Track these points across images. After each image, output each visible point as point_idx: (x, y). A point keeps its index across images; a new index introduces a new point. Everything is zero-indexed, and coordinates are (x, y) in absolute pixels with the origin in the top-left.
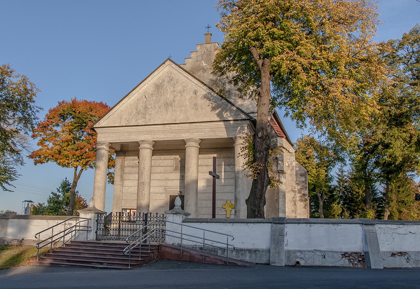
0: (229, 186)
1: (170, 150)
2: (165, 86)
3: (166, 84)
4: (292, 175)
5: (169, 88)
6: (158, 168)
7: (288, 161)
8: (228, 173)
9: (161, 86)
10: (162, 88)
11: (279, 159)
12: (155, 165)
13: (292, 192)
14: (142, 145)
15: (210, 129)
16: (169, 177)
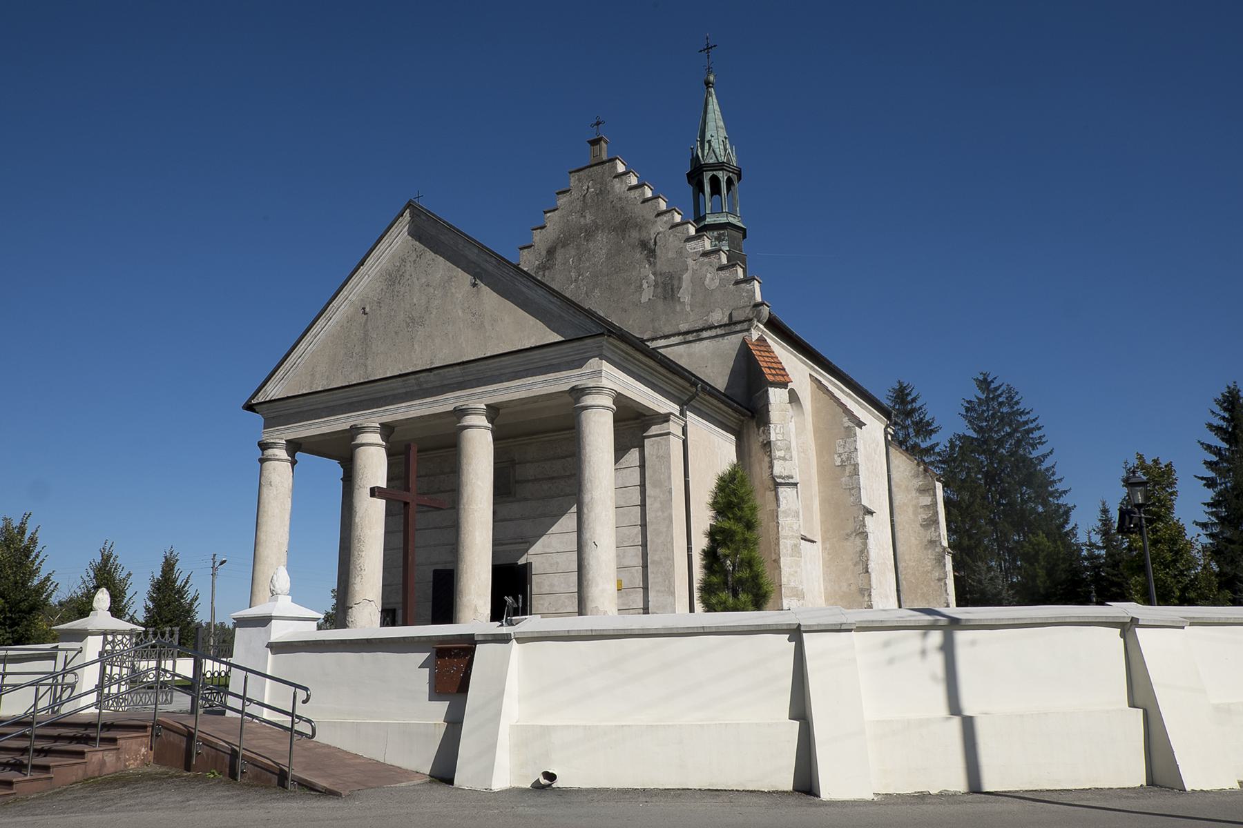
2: (407, 276)
3: (409, 269)
4: (853, 489)
5: (416, 279)
7: (841, 451)
9: (398, 276)
10: (402, 282)
11: (775, 445)
13: (858, 537)
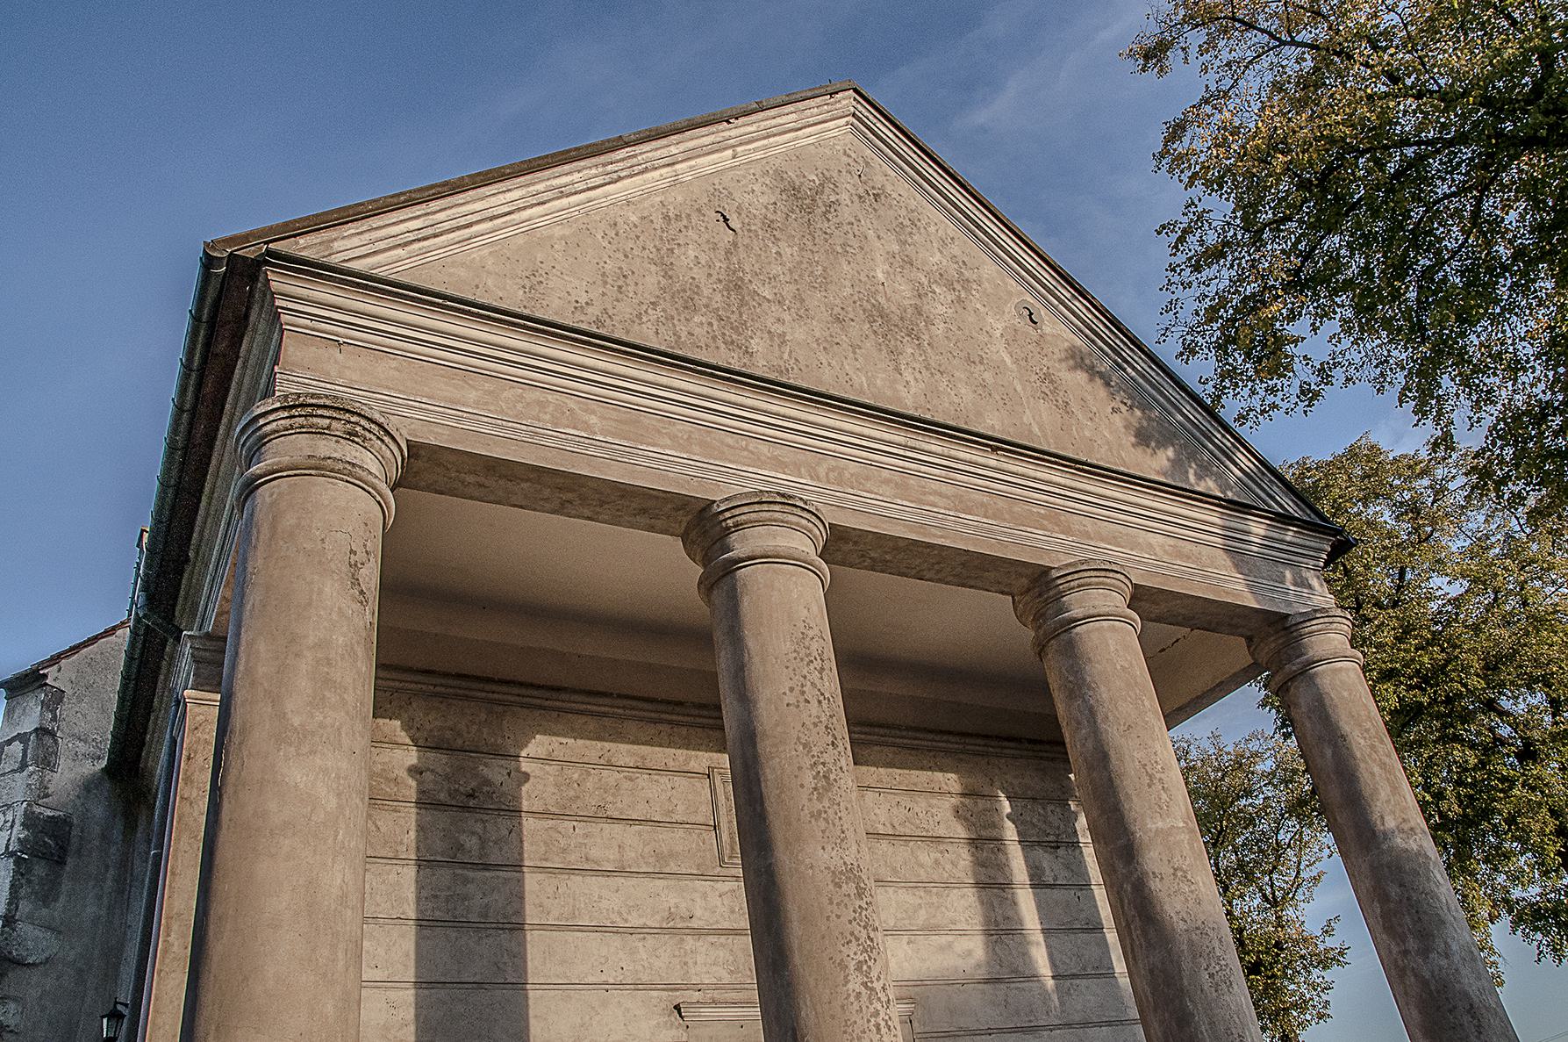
0: (1087, 976)
1: (680, 704)
6: (593, 828)
8: (1056, 894)
12: (574, 809)
14: (745, 538)
15: (1171, 541)
16: (698, 913)
